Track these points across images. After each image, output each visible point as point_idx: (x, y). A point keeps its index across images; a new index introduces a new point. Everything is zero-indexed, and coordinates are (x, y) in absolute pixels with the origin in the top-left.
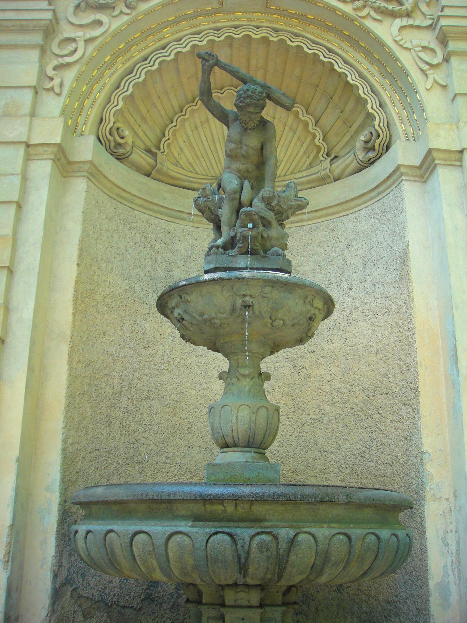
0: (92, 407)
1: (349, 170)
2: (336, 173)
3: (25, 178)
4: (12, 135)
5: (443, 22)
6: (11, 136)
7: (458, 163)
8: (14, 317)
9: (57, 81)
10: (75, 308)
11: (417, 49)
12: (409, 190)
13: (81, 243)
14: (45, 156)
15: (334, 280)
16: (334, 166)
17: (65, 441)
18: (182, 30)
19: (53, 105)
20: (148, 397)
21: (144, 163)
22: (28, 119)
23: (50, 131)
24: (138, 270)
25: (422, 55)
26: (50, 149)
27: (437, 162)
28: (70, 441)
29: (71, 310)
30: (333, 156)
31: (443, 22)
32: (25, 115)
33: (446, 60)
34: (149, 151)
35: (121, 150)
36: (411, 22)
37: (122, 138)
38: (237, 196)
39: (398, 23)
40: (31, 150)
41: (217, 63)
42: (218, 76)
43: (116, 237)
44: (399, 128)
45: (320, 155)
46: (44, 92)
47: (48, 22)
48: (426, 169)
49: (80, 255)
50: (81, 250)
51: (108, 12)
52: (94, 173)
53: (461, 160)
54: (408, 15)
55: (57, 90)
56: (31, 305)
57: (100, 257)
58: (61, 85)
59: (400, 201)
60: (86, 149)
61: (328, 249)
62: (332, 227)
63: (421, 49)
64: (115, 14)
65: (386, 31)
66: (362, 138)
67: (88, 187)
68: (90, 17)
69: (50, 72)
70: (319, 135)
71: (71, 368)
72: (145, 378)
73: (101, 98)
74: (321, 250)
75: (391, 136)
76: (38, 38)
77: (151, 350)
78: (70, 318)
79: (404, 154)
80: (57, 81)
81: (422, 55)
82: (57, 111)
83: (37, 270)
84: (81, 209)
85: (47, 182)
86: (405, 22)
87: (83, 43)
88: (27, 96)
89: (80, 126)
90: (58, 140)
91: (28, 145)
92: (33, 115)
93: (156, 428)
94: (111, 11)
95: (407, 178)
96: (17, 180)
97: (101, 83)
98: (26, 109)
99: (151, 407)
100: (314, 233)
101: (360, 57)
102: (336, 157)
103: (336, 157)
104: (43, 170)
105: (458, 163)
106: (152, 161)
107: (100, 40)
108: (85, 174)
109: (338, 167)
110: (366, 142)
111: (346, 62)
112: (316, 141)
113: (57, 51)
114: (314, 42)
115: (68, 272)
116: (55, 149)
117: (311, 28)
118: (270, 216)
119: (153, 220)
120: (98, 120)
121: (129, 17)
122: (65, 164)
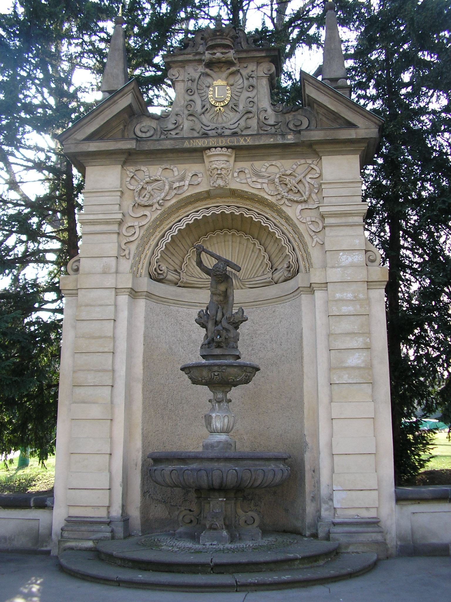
0: (154, 411)
1: (281, 279)
2: (276, 279)
3: (116, 306)
4: (108, 284)
5: (322, 209)
6: (108, 285)
7: (326, 289)
8: (117, 374)
9: (127, 252)
10: (144, 366)
11: (309, 223)
12: (305, 298)
13: (144, 334)
14: (125, 293)
15: (274, 339)
16: (274, 276)
17: (143, 429)
18: (189, 211)
19: (126, 265)
20: (181, 403)
21: (174, 279)
22: (115, 275)
23: (126, 282)
24: (173, 338)
25: (312, 227)
26: (126, 290)
27: (315, 289)
28: (145, 429)
29: (142, 367)
30: (274, 269)
31: (322, 209)
32: (113, 273)
33: (324, 228)
34: (176, 271)
35: (161, 277)
36: (307, 207)
37: (161, 271)
38: (215, 317)
39: (300, 207)
40: (117, 290)
41: (204, 250)
42: (204, 256)
43: (161, 323)
44: (302, 268)
45: (267, 269)
46: (121, 257)
47: (120, 220)
48: (311, 289)
49: (145, 340)
50: (144, 337)
51: (150, 208)
52: (149, 295)
53: (327, 287)
54: (305, 202)
55: (128, 257)
56: (124, 369)
57: (154, 336)
58: (129, 253)
59: (299, 306)
60: (145, 284)
61: (271, 322)
62: (273, 310)
63: (311, 223)
64: (153, 210)
65: (293, 212)
66: (286, 266)
67: (146, 303)
68: (141, 212)
69: (124, 247)
70: (267, 257)
71: (143, 394)
72: (180, 393)
73: (149, 253)
74: (268, 322)
75: (299, 267)
76: (115, 227)
77: (182, 379)
78: (142, 372)
79: (300, 280)
80: (127, 252)
81: (312, 227)
82: (128, 269)
83: (125, 351)
84: (143, 316)
85: (126, 307)
86: (304, 206)
87: (138, 229)
88: (114, 260)
89: (140, 269)
90: (130, 286)
91: (116, 288)
92: (117, 272)
93: (186, 418)
94: (151, 208)
95: (304, 293)
96: (112, 308)
97: (149, 245)
98: (113, 270)
99: (183, 407)
100: (265, 312)
101: (267, 210)
102: (276, 269)
103: (276, 269)
104: (124, 299)
105: (326, 289)
106: (178, 277)
107: (147, 226)
108: (144, 297)
109: (277, 276)
110: (288, 267)
111: (275, 225)
112: (265, 260)
113: (126, 234)
114: (259, 214)
115: (139, 349)
116: (129, 290)
117: (257, 205)
118: (230, 327)
119: (181, 309)
120: (148, 265)
121: (161, 211)
122: (134, 293)
